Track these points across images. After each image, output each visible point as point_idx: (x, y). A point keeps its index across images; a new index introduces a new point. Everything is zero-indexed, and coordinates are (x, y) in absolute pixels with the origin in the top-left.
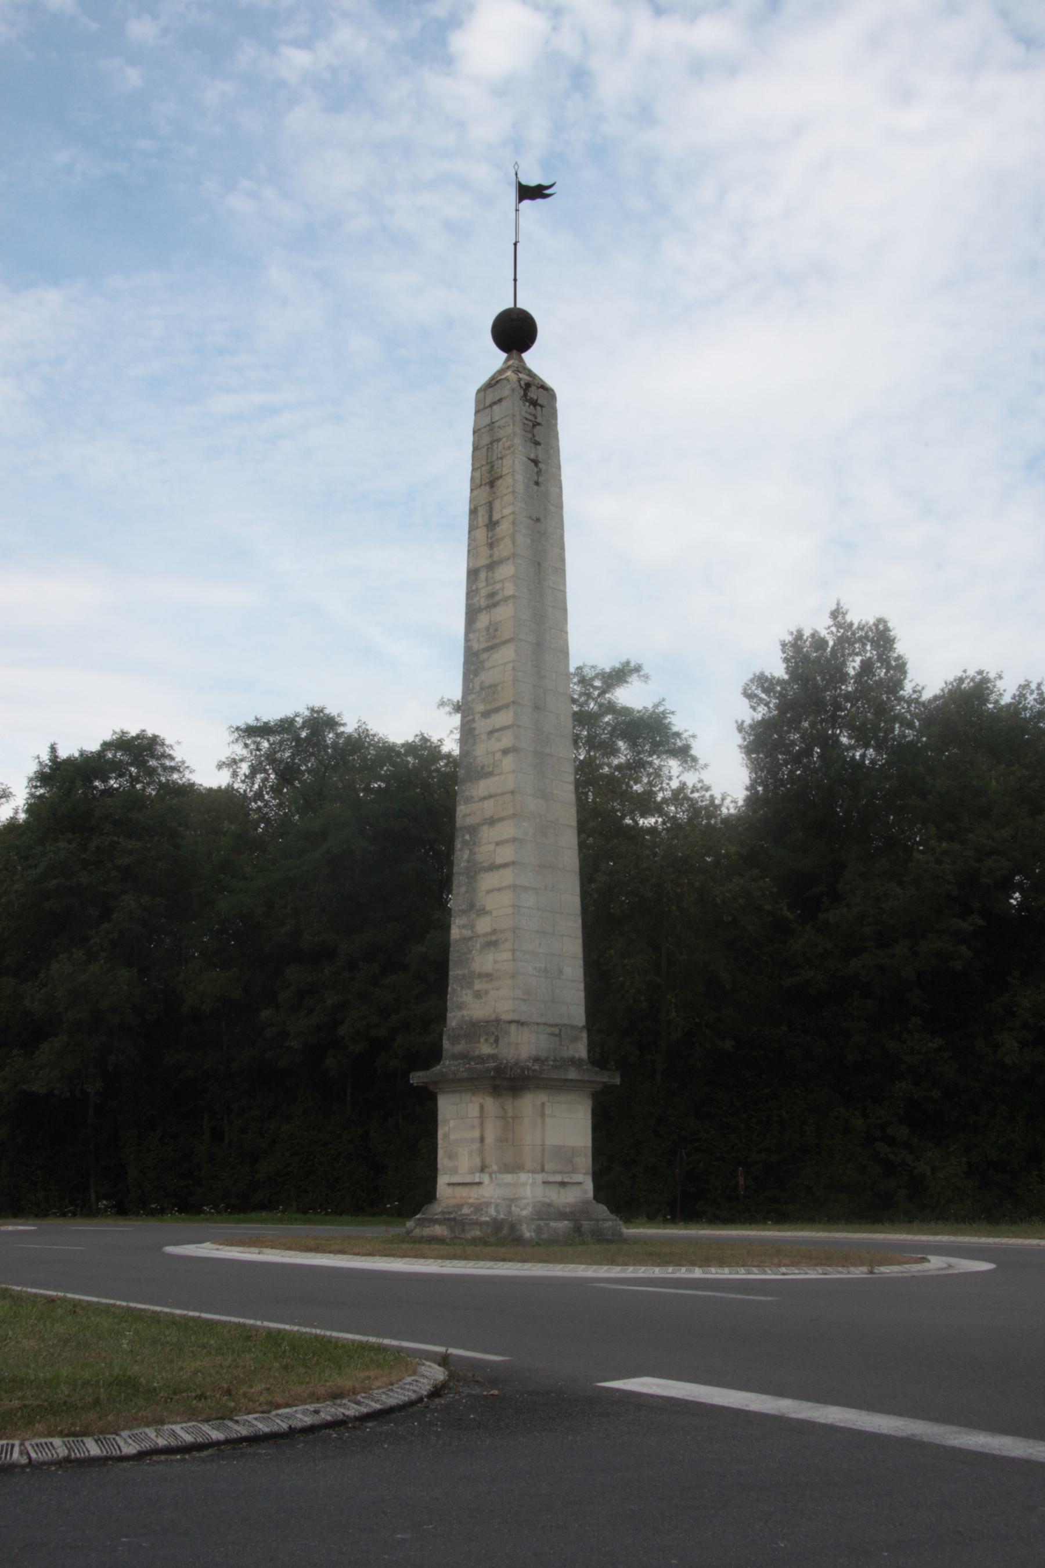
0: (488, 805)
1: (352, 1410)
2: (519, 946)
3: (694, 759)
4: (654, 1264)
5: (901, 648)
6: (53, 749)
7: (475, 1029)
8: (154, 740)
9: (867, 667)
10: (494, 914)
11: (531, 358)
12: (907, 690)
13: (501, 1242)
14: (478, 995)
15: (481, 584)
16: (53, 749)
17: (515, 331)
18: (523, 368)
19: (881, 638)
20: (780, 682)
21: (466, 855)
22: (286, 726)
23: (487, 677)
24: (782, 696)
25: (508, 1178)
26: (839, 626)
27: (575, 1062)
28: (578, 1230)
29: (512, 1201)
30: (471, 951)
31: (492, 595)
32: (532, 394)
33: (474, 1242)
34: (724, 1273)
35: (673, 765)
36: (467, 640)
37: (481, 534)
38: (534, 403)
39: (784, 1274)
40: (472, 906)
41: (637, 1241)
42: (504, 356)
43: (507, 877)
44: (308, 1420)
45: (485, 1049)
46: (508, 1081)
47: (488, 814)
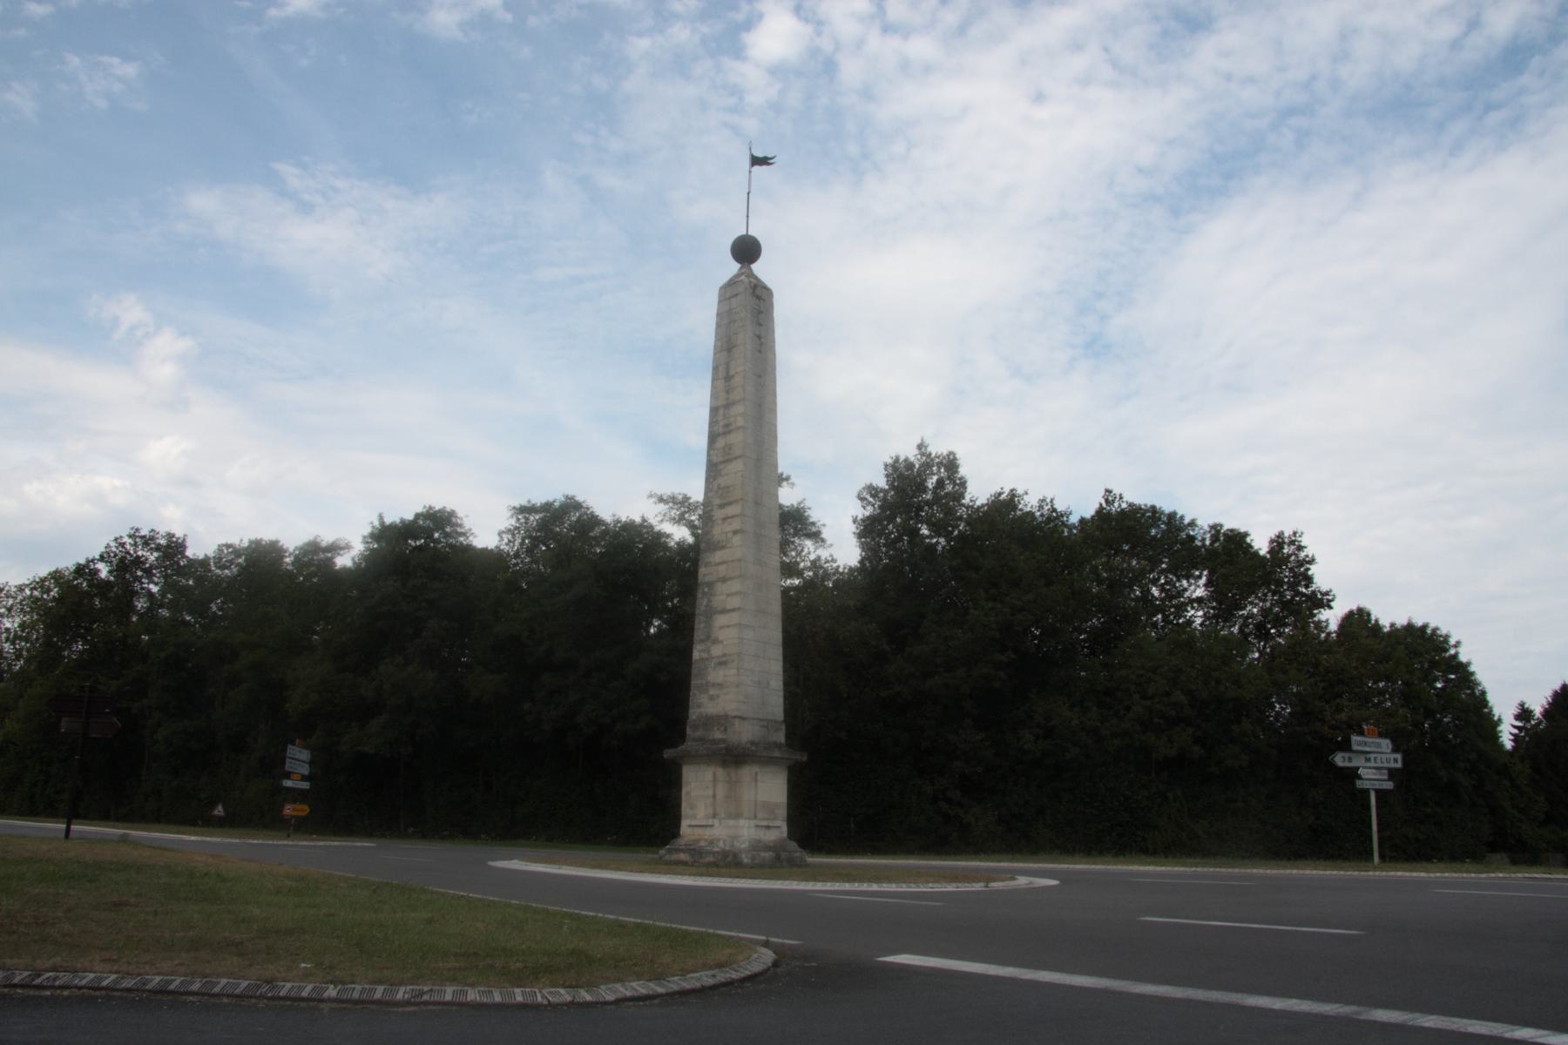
0: (722, 568)
1: (735, 975)
2: (740, 669)
3: (823, 540)
4: (848, 881)
5: (963, 471)
6: (381, 518)
7: (710, 721)
8: (452, 514)
9: (940, 483)
11: (756, 267)
12: (966, 501)
13: (727, 866)
14: (712, 698)
15: (720, 418)
16: (381, 518)
17: (746, 250)
18: (751, 275)
19: (951, 464)
20: (882, 490)
21: (705, 602)
22: (547, 507)
23: (722, 481)
24: (884, 500)
25: (731, 822)
26: (923, 454)
27: (777, 746)
28: (778, 858)
29: (734, 838)
31: (727, 425)
32: (758, 292)
33: (709, 865)
34: (893, 888)
35: (808, 543)
36: (709, 455)
37: (721, 383)
38: (759, 298)
40: (708, 637)
41: (815, 866)
43: (734, 618)
44: (711, 982)
45: (718, 735)
46: (734, 757)
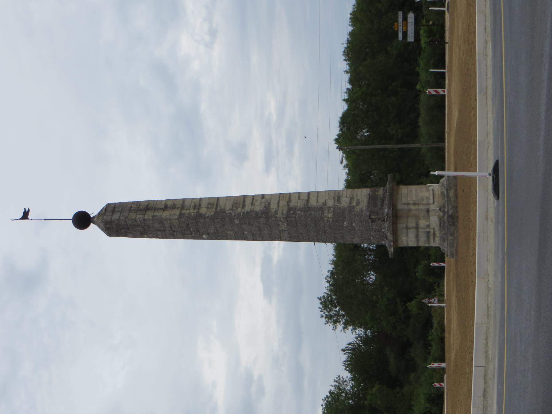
0: (281, 204)
10: (327, 198)
14: (358, 203)
17: (82, 220)
30: (340, 208)
39: (494, 375)
42: (92, 225)
47: (285, 203)
